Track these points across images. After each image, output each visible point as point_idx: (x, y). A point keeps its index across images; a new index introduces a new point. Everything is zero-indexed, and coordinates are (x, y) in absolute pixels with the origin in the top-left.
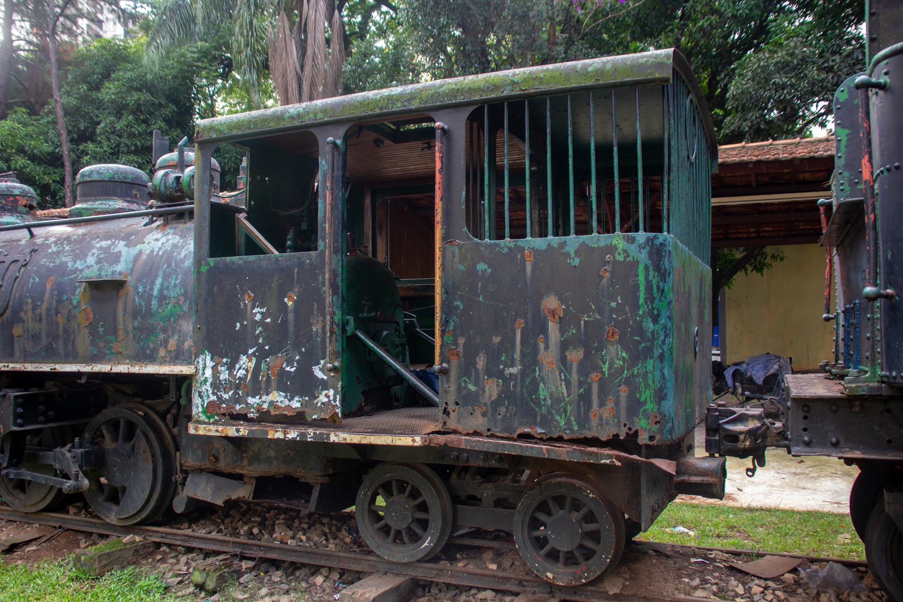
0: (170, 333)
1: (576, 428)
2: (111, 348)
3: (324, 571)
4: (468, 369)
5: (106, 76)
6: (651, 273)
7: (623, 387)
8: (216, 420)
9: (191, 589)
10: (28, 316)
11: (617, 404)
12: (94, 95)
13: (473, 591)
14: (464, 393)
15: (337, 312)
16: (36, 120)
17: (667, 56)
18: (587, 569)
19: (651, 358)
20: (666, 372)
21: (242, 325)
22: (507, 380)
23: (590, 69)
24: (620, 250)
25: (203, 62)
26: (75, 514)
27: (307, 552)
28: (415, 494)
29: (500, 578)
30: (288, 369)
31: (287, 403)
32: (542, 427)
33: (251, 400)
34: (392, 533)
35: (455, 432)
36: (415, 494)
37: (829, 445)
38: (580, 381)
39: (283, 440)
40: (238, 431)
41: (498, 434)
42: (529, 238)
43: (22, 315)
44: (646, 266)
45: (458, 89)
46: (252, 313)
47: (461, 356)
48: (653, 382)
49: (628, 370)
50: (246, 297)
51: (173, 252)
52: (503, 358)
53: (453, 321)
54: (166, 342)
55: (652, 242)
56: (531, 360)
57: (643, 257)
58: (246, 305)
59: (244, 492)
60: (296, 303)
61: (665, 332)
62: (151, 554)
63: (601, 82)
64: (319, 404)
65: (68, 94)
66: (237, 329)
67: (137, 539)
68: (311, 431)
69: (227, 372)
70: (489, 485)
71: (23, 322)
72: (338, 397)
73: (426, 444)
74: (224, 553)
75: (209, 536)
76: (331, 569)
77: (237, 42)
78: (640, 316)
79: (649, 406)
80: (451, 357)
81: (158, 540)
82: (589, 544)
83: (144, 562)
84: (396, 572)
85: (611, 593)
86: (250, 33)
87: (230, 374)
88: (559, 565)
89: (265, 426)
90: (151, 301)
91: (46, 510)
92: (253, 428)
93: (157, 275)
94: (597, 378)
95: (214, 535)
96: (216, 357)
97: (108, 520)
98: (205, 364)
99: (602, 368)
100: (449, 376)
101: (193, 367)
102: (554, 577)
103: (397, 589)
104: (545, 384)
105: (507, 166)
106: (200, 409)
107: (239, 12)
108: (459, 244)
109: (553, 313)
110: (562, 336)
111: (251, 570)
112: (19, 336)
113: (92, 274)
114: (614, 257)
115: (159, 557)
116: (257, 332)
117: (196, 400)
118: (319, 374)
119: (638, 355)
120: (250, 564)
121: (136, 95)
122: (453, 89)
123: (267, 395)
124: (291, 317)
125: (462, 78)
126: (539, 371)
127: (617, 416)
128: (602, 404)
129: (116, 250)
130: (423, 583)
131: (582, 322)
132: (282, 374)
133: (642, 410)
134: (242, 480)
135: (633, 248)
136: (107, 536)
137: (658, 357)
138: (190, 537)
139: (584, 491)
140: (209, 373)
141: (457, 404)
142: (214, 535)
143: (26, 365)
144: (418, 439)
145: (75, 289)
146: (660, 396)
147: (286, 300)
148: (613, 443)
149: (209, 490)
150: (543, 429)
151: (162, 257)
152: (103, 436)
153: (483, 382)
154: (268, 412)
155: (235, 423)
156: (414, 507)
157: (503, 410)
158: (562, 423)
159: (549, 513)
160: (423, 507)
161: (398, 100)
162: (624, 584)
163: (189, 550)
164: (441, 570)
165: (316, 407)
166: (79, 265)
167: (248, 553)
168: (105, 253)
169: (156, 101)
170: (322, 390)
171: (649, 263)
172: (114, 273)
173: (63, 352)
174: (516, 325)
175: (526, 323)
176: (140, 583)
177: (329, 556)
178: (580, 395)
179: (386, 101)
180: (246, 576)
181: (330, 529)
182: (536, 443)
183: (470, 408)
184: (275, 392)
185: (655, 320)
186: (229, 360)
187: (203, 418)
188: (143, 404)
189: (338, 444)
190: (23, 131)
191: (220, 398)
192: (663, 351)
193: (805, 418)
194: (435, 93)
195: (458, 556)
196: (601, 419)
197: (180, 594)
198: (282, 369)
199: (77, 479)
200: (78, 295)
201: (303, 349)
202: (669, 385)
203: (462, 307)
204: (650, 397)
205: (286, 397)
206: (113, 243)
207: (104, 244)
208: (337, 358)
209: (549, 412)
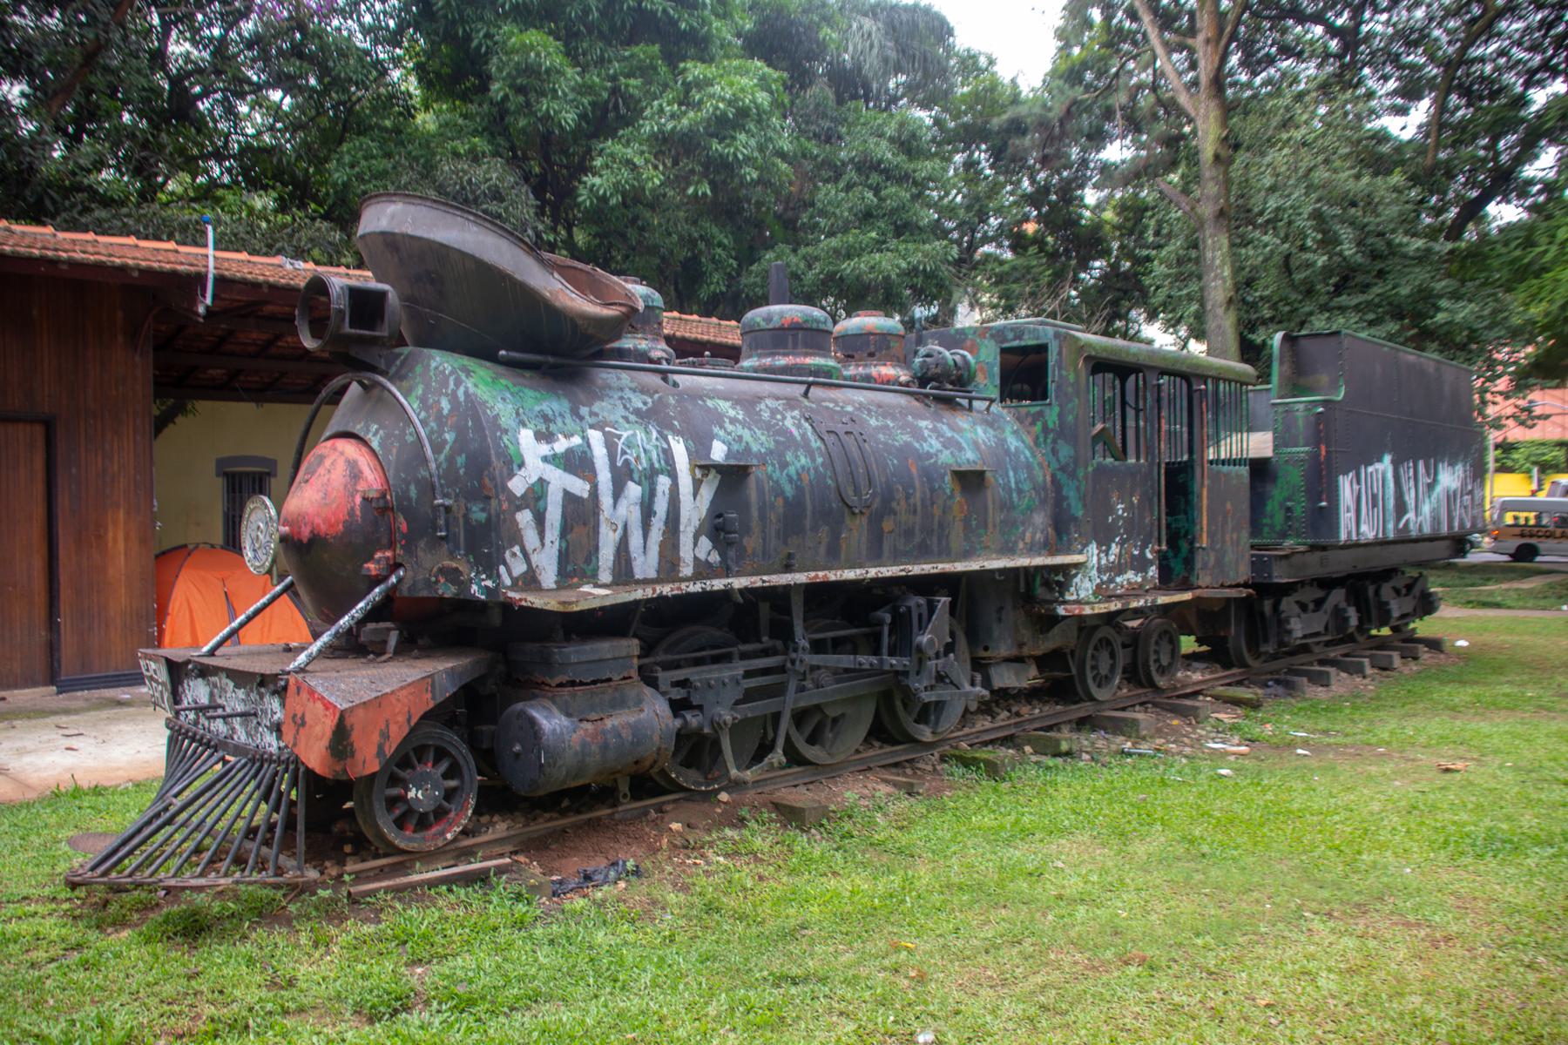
10: (900, 506)
33: (1118, 580)
43: (894, 505)
71: (895, 514)
74: (1179, 697)
132: (1132, 556)
140: (1095, 559)
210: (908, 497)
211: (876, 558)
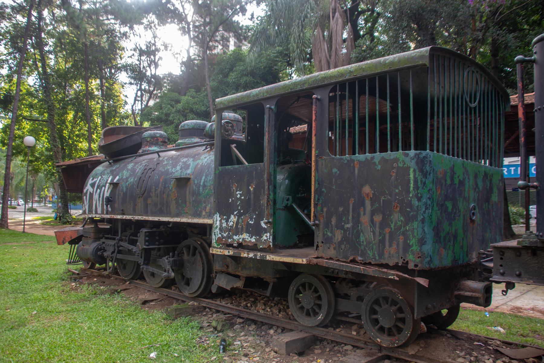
0: (207, 203)
1: (377, 258)
2: (184, 210)
3: (275, 328)
4: (328, 224)
5: (231, 70)
6: (417, 173)
7: (401, 237)
9: (212, 329)
11: (398, 245)
12: (225, 80)
13: (343, 345)
14: (326, 237)
15: (271, 194)
16: (199, 95)
17: (426, 51)
18: (398, 339)
19: (416, 221)
20: (426, 229)
21: (232, 200)
22: (345, 230)
23: (387, 62)
24: (401, 161)
25: (279, 58)
26: (174, 290)
27: (267, 317)
28: (316, 291)
29: (355, 339)
30: (250, 222)
31: (250, 239)
32: (361, 256)
33: (235, 237)
34: (305, 310)
35: (322, 258)
36: (316, 291)
37: (515, 275)
38: (380, 233)
39: (247, 258)
40: (229, 252)
42: (357, 155)
43: (151, 194)
44: (414, 169)
48: (417, 234)
49: (404, 227)
50: (234, 186)
51: (211, 164)
52: (344, 219)
54: (205, 207)
55: (418, 156)
56: (357, 221)
57: (412, 165)
58: (234, 190)
59: (239, 284)
60: (254, 188)
61: (426, 207)
62: (202, 312)
63: (392, 68)
65: (213, 80)
67: (195, 304)
68: (259, 254)
69: (225, 223)
70: (355, 289)
72: (271, 237)
73: (308, 263)
74: (229, 314)
75: (226, 305)
76: (278, 327)
77: (292, 46)
78: (410, 197)
79: (414, 248)
80: (320, 218)
81: (205, 305)
82: (400, 325)
83: (197, 315)
84: (306, 331)
85: (410, 354)
87: (227, 224)
88: (385, 335)
89: (240, 251)
90: (200, 187)
91: (161, 287)
93: (203, 175)
94: (389, 231)
95: (229, 305)
96: (221, 216)
97: (185, 294)
99: (391, 226)
101: (212, 220)
102: (381, 342)
103: (303, 339)
104: (363, 234)
105: (347, 117)
107: (293, 30)
108: (325, 159)
109: (368, 195)
110: (372, 208)
111: (240, 323)
112: (150, 204)
113: (178, 175)
114: (398, 164)
115: (205, 313)
117: (213, 237)
118: (264, 225)
119: (409, 219)
120: (241, 320)
121: (245, 78)
122: (323, 77)
123: (242, 235)
124: (252, 196)
125: (327, 71)
126: (361, 226)
127: (398, 252)
128: (390, 246)
129: (189, 163)
130: (320, 338)
131: (382, 200)
132: (248, 224)
133: (410, 250)
134: (239, 278)
135: (407, 160)
136: (185, 302)
137: (421, 220)
138: (218, 305)
139: (397, 295)
140: (218, 223)
141: (323, 242)
142: (229, 305)
143: (150, 217)
144: (304, 260)
145: (171, 181)
146: (422, 242)
147: (250, 187)
148: (396, 267)
150: (362, 258)
151: (206, 166)
152: (183, 253)
155: (228, 248)
156: (316, 297)
157: (343, 247)
158: (371, 254)
159: (380, 306)
160: (319, 298)
161: (299, 85)
162: (419, 350)
163: (218, 311)
164: (328, 332)
166: (173, 170)
167: (242, 315)
168: (184, 164)
169: (255, 81)
171: (416, 167)
172: (186, 174)
173: (165, 212)
174: (350, 201)
175: (355, 200)
176: (191, 324)
177: (277, 320)
178: (380, 240)
180: (237, 326)
181: (284, 307)
182: (358, 265)
183: (328, 245)
184: (245, 234)
185: (419, 200)
187: (216, 245)
188: (201, 238)
189: (270, 261)
190: (193, 101)
191: (222, 236)
192: (424, 217)
193: (502, 259)
195: (341, 326)
196: (390, 254)
197: (206, 331)
199: (168, 272)
200: (172, 184)
202: (428, 236)
203: (325, 192)
204: (415, 243)
205: (249, 236)
206: (188, 160)
207: (185, 160)
208: (271, 217)
209: (365, 249)
210: (156, 190)
211: (146, 213)
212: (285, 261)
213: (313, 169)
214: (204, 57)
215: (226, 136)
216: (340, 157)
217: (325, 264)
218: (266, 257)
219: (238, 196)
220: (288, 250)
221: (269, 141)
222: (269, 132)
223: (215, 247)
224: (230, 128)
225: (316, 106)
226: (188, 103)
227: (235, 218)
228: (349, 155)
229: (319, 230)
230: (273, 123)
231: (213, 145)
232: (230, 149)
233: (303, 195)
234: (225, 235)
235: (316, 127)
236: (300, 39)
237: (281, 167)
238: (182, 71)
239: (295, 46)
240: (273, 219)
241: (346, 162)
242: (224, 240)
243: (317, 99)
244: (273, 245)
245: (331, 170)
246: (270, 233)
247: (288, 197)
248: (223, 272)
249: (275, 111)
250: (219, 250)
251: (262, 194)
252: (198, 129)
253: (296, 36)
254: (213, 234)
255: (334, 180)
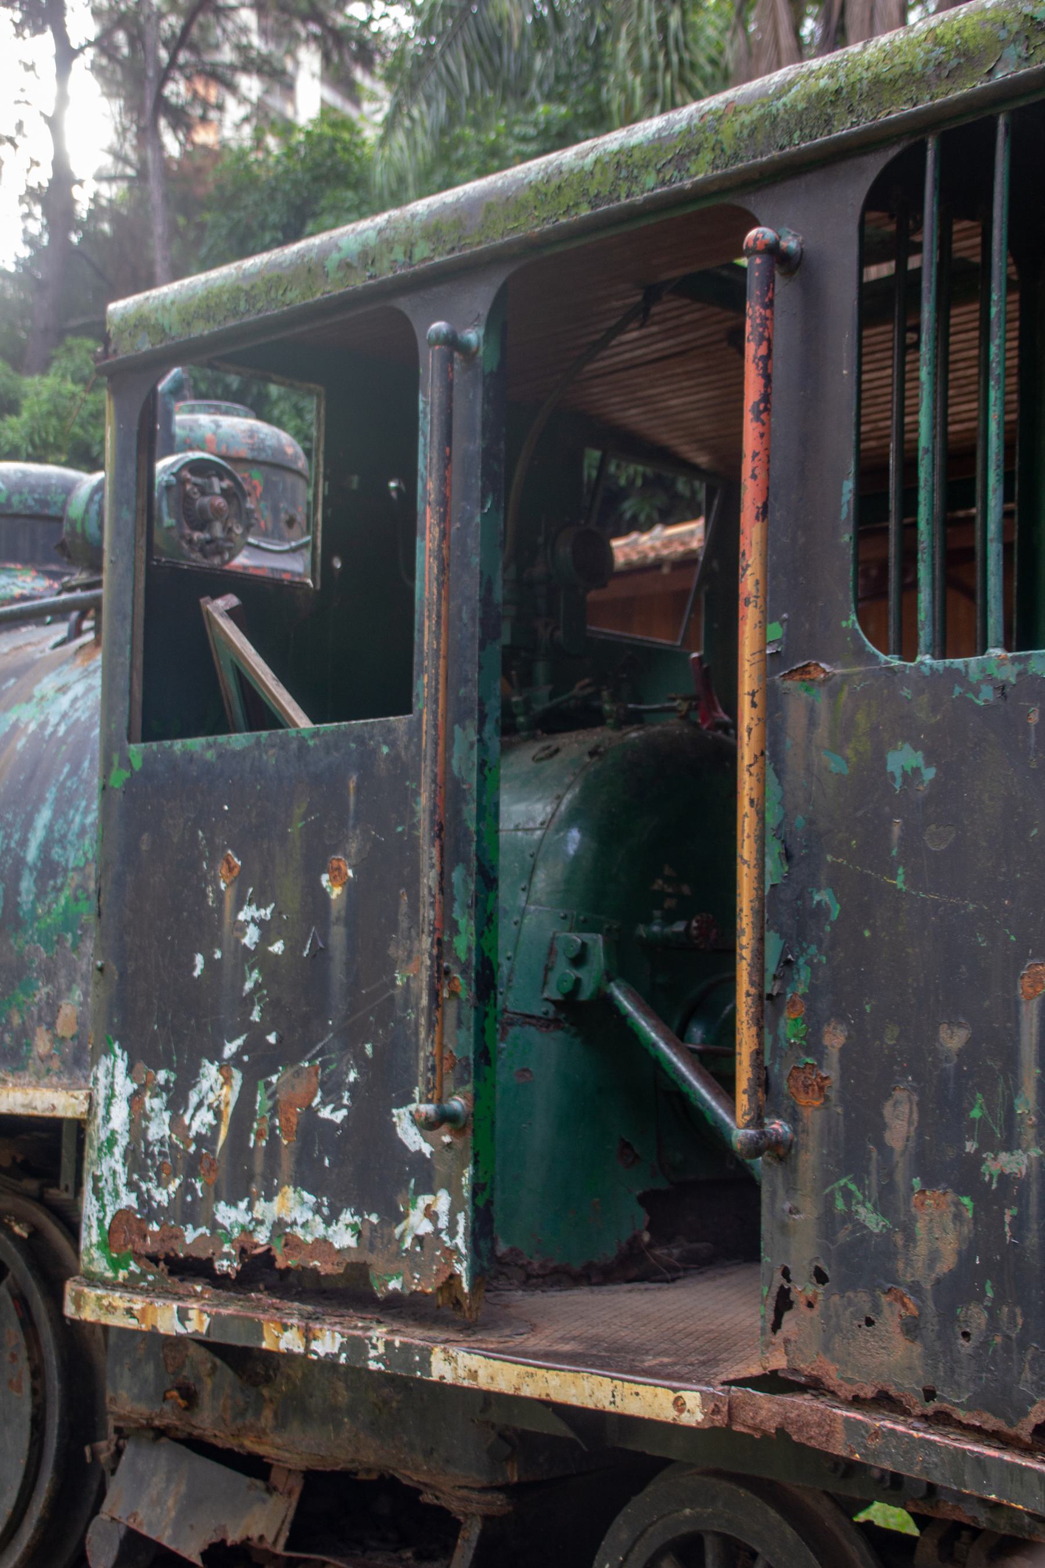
0: (63, 981)
8: (132, 1274)
14: (843, 1236)
21: (209, 961)
30: (325, 1113)
35: (815, 1386)
40: (183, 1316)
41: (962, 1415)
45: (838, 92)
46: (236, 921)
47: (833, 1095)
50: (222, 869)
52: (976, 1113)
53: (809, 963)
54: (53, 1007)
58: (219, 895)
60: (351, 887)
64: (408, 1243)
66: (197, 973)
68: (379, 1334)
69: (166, 1116)
72: (461, 1218)
73: (720, 1420)
77: (623, 88)
80: (803, 1099)
86: (661, 59)
87: (175, 1122)
89: (259, 1306)
92: (224, 1312)
93: (41, 799)
96: (141, 1066)
98: (112, 1086)
100: (794, 1170)
106: (95, 1238)
108: (829, 678)
116: (249, 986)
117: (90, 1207)
118: (412, 1138)
122: (821, 94)
123: (269, 1199)
124: (338, 934)
140: (120, 1114)
141: (820, 1277)
147: (325, 879)
149: (170, 1502)
151: (63, 741)
153: (907, 1201)
154: (268, 1258)
157: (977, 1318)
161: (646, 165)
165: (399, 1250)
170: (417, 1193)
179: (611, 175)
183: (862, 1299)
184: (289, 1190)
186: (173, 1077)
187: (100, 1265)
189: (456, 1390)
191: (145, 1200)
194: (762, 118)
198: (311, 1112)
201: (369, 1048)
203: (835, 913)
205: (317, 1210)
208: (461, 1082)
212: (559, 1396)
213: (747, 750)
214: (143, 161)
215: (196, 556)
216: (939, 664)
217: (840, 1436)
218: (426, 1364)
219: (251, 937)
220: (581, 1297)
221: (444, 567)
222: (444, 501)
223: (94, 1280)
224: (220, 501)
225: (769, 305)
226: (56, 413)
227: (227, 1080)
228: (1008, 648)
229: (791, 1188)
230: (476, 445)
231: (95, 604)
232: (201, 624)
233: (679, 927)
234: (161, 1196)
235: (768, 457)
236: (664, 43)
237: (535, 749)
238: (30, 241)
239: (637, 83)
240: (476, 1097)
241: (987, 695)
242: (155, 1227)
243: (773, 252)
244: (477, 1275)
245: (880, 758)
246: (454, 1191)
247: (577, 938)
248: (161, 1433)
249: (488, 360)
250: (118, 1299)
251: (404, 924)
252: (33, 517)
253: (643, 30)
254: (88, 1186)
255: (896, 830)
